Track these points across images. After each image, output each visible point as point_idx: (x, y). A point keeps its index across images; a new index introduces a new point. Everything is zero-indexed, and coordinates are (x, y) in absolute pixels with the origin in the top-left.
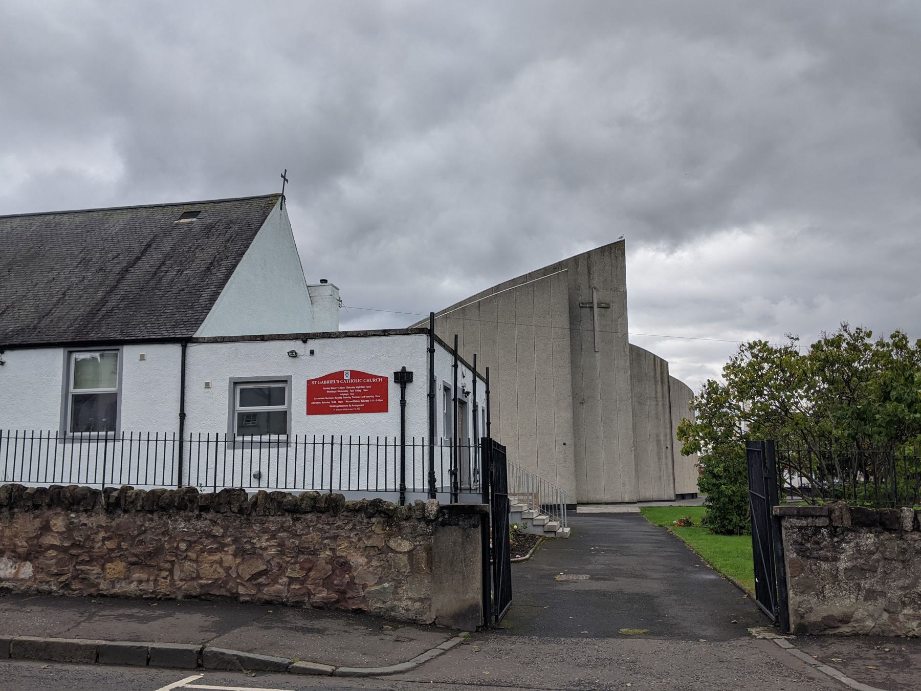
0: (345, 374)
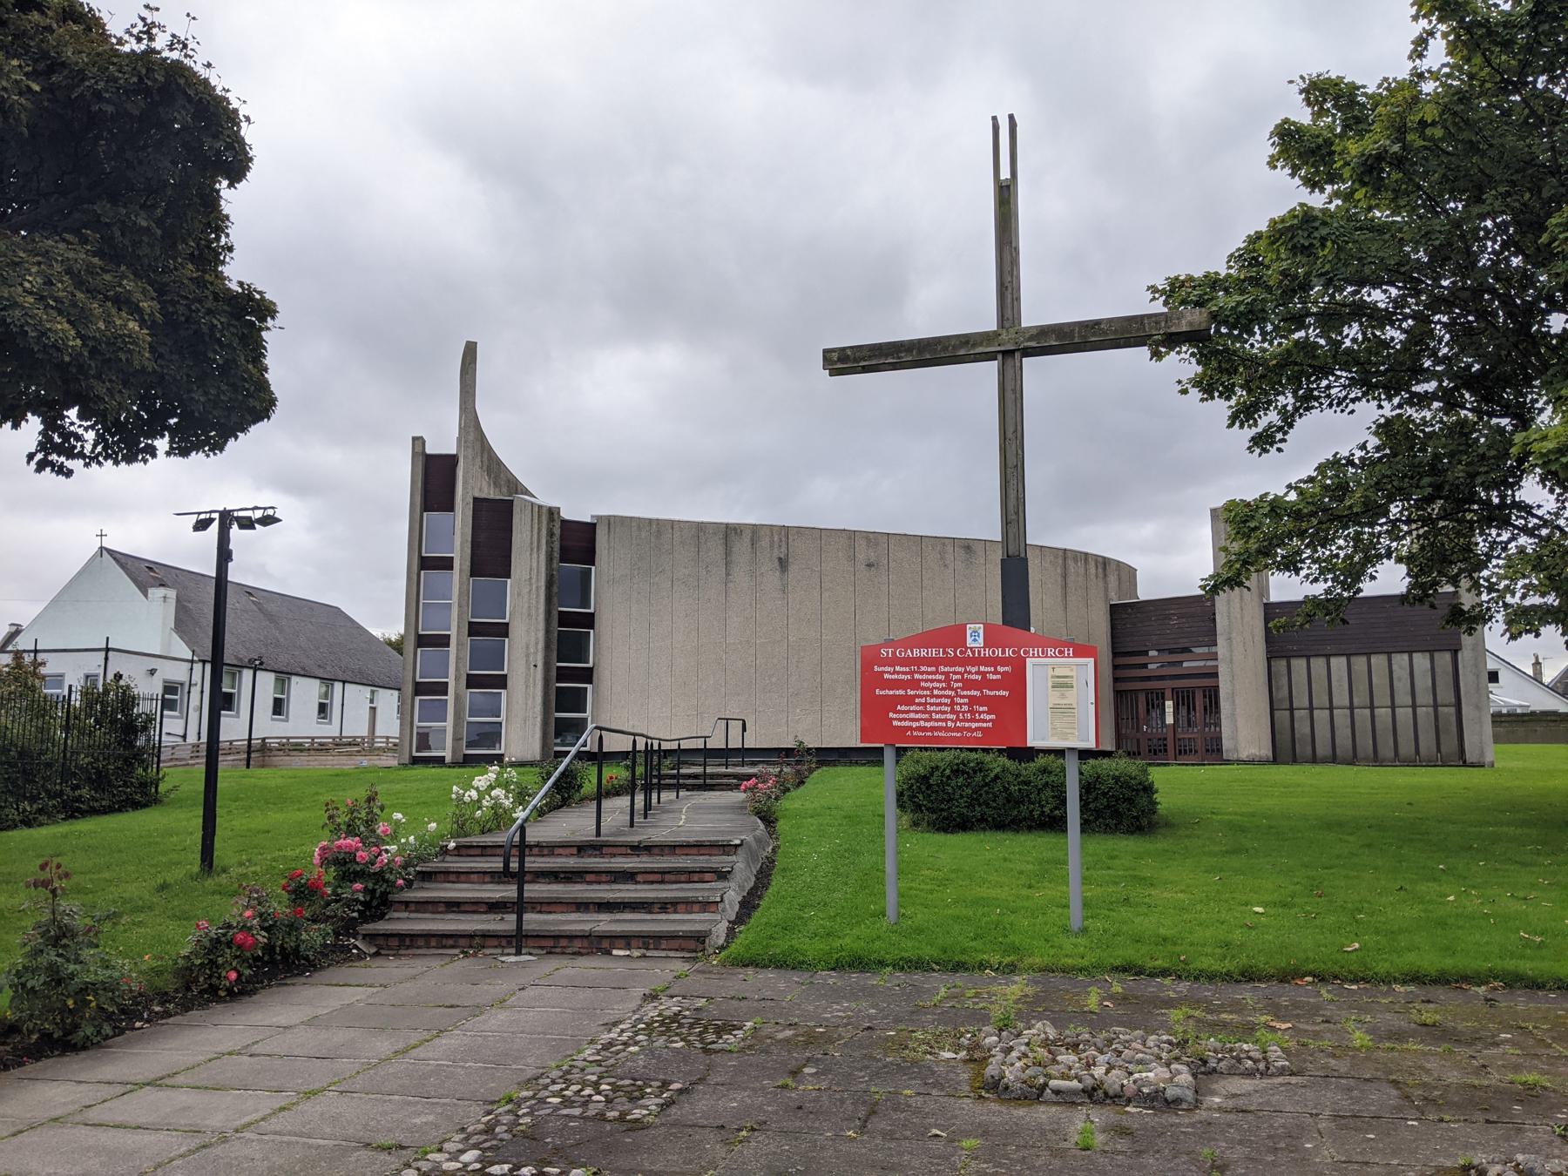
0: (969, 632)
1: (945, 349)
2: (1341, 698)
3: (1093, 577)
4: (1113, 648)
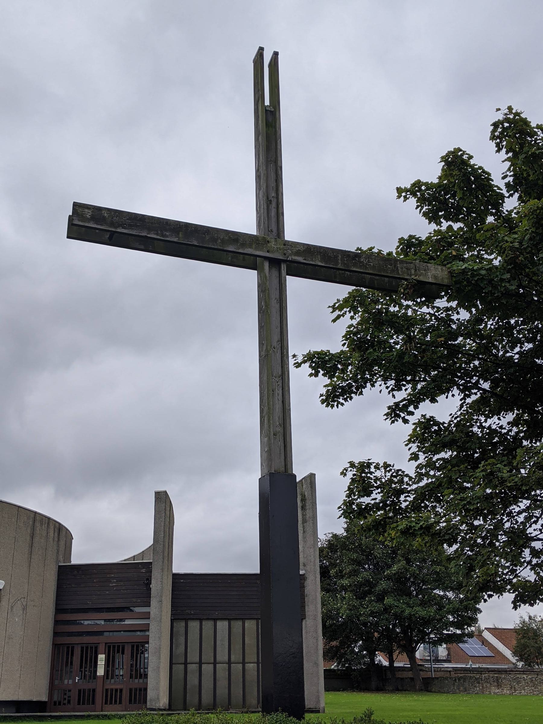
1: (214, 240)
2: (222, 656)
3: (51, 540)
4: (57, 604)
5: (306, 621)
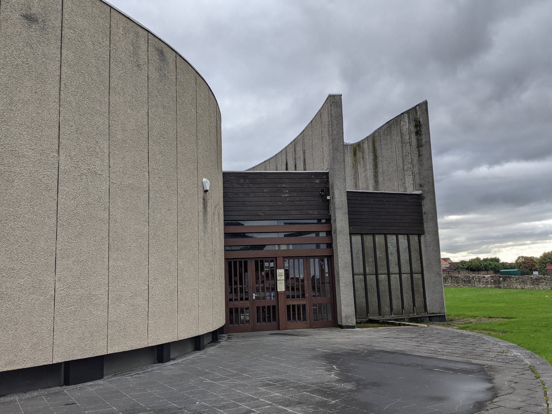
2: (405, 268)
5: (425, 236)
